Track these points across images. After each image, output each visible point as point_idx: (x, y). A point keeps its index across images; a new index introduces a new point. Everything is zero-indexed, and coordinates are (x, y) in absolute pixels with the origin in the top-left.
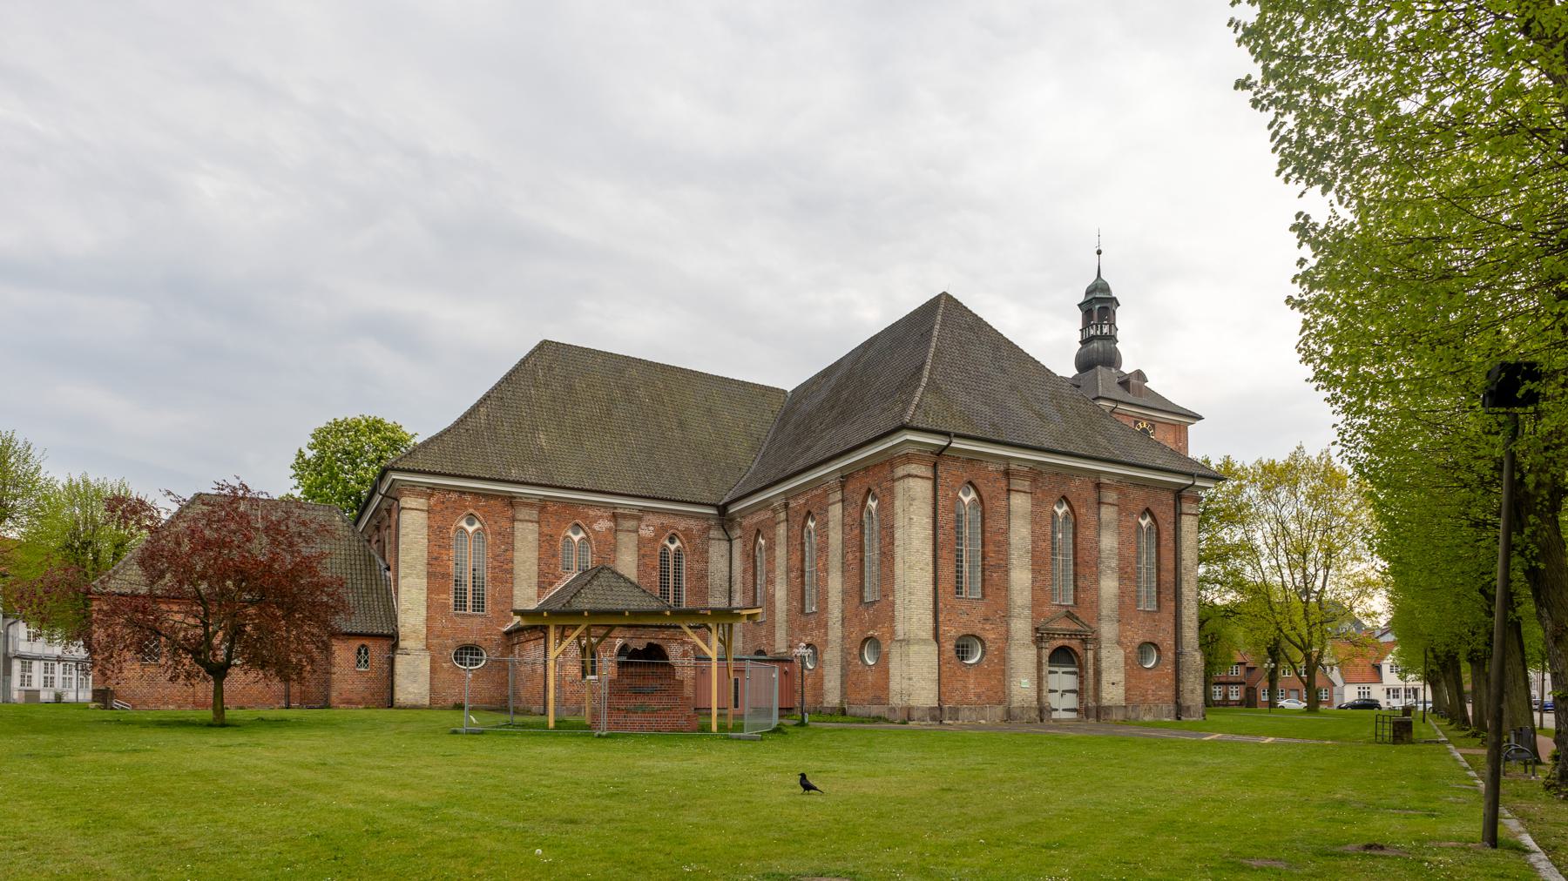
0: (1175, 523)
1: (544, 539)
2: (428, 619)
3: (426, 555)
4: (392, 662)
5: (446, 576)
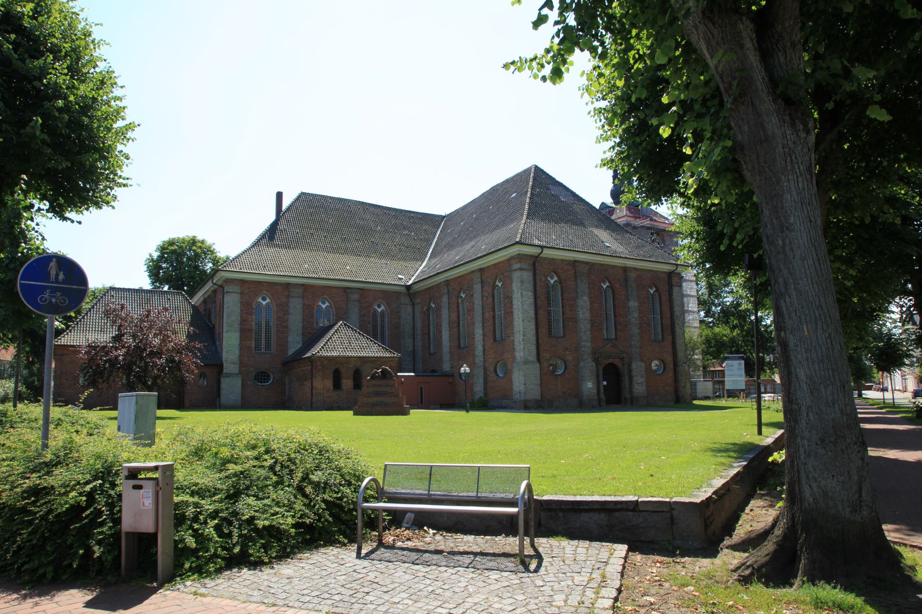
0: (669, 291)
2: (240, 356)
3: (239, 318)
4: (219, 383)
5: (250, 330)
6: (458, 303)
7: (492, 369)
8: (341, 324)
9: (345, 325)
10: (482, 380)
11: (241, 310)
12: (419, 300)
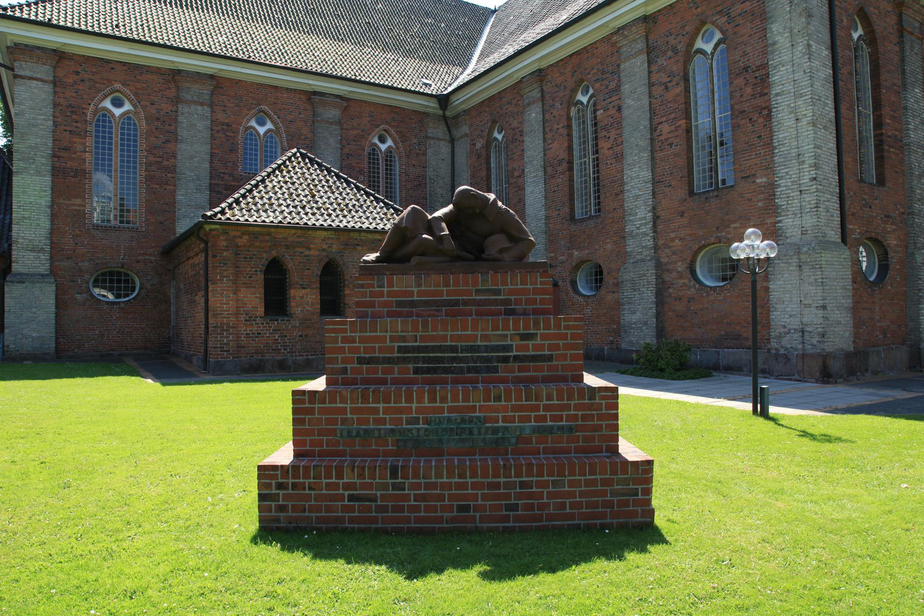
1: (219, 128)
2: (53, 232)
3: (50, 144)
6: (569, 119)
7: (681, 267)
8: (294, 155)
9: (303, 156)
10: (649, 295)
11: (55, 124)
12: (465, 129)
